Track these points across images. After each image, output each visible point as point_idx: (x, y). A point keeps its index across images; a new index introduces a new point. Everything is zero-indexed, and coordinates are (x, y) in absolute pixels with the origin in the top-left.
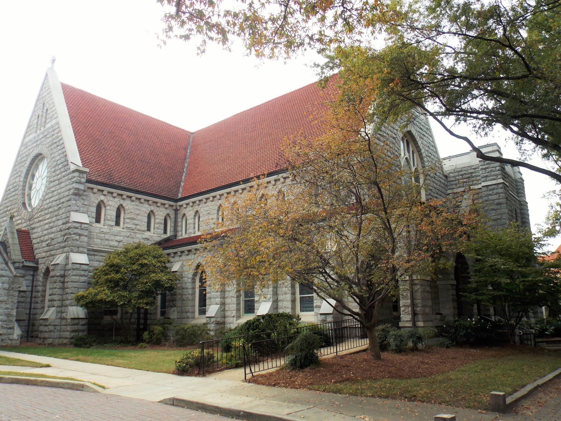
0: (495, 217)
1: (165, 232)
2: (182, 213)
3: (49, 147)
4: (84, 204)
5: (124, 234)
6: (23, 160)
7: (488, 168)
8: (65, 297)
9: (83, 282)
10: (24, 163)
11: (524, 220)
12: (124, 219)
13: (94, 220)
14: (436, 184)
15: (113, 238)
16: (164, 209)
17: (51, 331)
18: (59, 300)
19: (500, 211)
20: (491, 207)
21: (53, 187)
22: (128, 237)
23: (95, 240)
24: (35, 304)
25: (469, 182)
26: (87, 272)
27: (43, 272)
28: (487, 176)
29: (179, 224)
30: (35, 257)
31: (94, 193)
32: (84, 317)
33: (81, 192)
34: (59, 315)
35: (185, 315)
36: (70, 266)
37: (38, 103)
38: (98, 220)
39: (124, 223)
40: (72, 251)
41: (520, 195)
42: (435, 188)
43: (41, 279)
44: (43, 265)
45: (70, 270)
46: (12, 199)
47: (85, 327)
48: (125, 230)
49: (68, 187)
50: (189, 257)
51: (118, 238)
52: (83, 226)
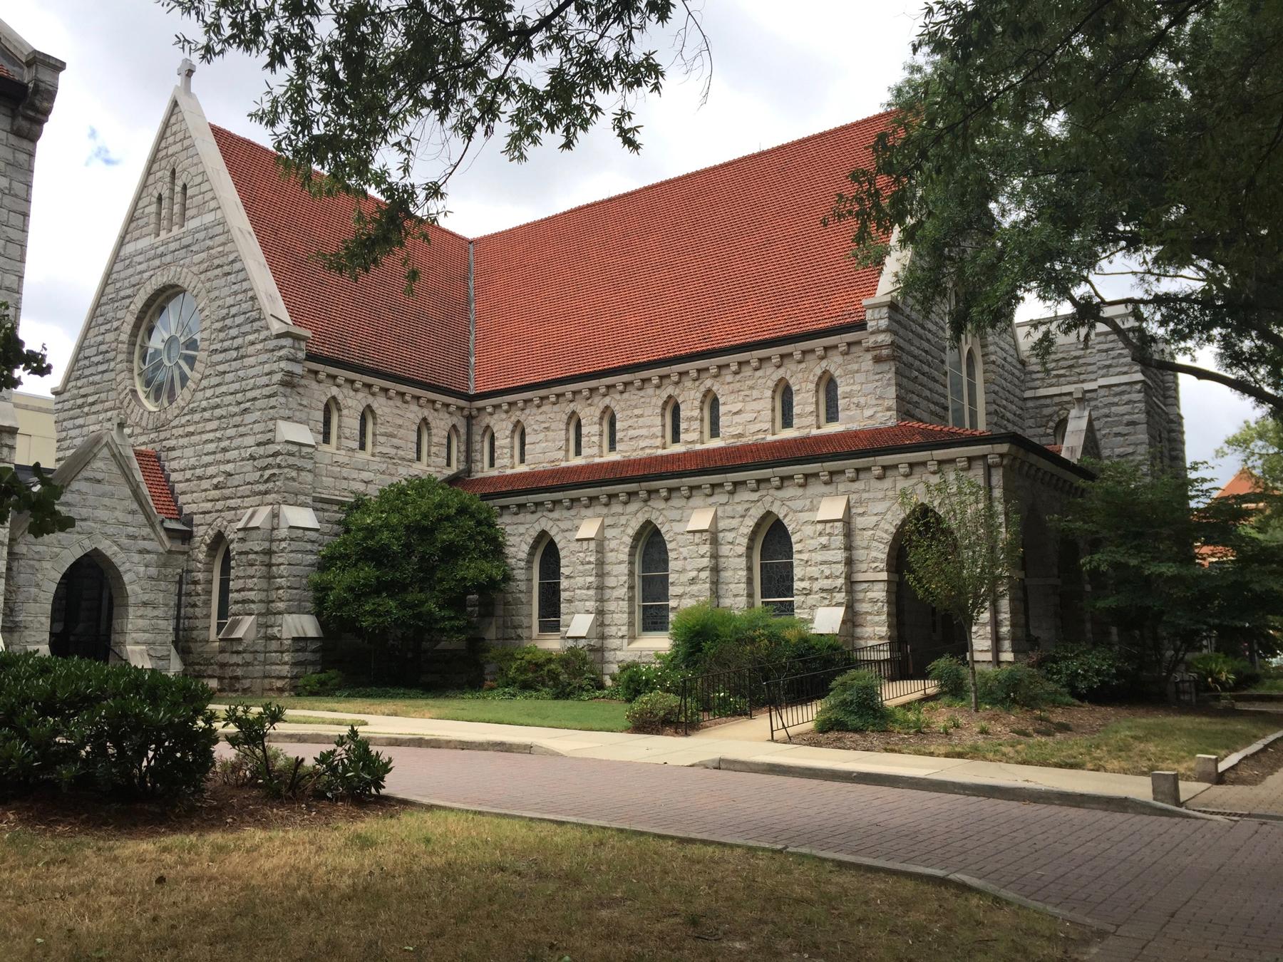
0: (1122, 450)
1: (449, 464)
2: (484, 424)
3: (201, 273)
4: (301, 405)
5: (376, 467)
6: (122, 294)
7: (1113, 349)
8: (274, 595)
9: (309, 566)
10: (128, 301)
11: (1174, 453)
12: (374, 435)
13: (321, 437)
14: (1005, 379)
15: (355, 474)
16: (447, 416)
17: (247, 664)
18: (261, 601)
19: (1132, 438)
20: (1116, 430)
21: (221, 363)
22: (383, 473)
23: (324, 479)
24: (188, 609)
25: (1071, 376)
26: (316, 545)
27: (209, 541)
28: (1109, 366)
29: (477, 446)
30: (180, 510)
31: (319, 382)
32: (316, 636)
33: (296, 380)
34: (263, 631)
35: (512, 633)
36: (283, 533)
37: (156, 167)
38: (326, 439)
39: (374, 444)
40: (286, 503)
41: (1170, 401)
42: (1003, 388)
43: (201, 557)
44: (205, 527)
45: (284, 540)
46: (97, 378)
47: (317, 656)
48: (377, 459)
49: (267, 368)
50: (521, 517)
51: (366, 475)
52: (305, 450)
